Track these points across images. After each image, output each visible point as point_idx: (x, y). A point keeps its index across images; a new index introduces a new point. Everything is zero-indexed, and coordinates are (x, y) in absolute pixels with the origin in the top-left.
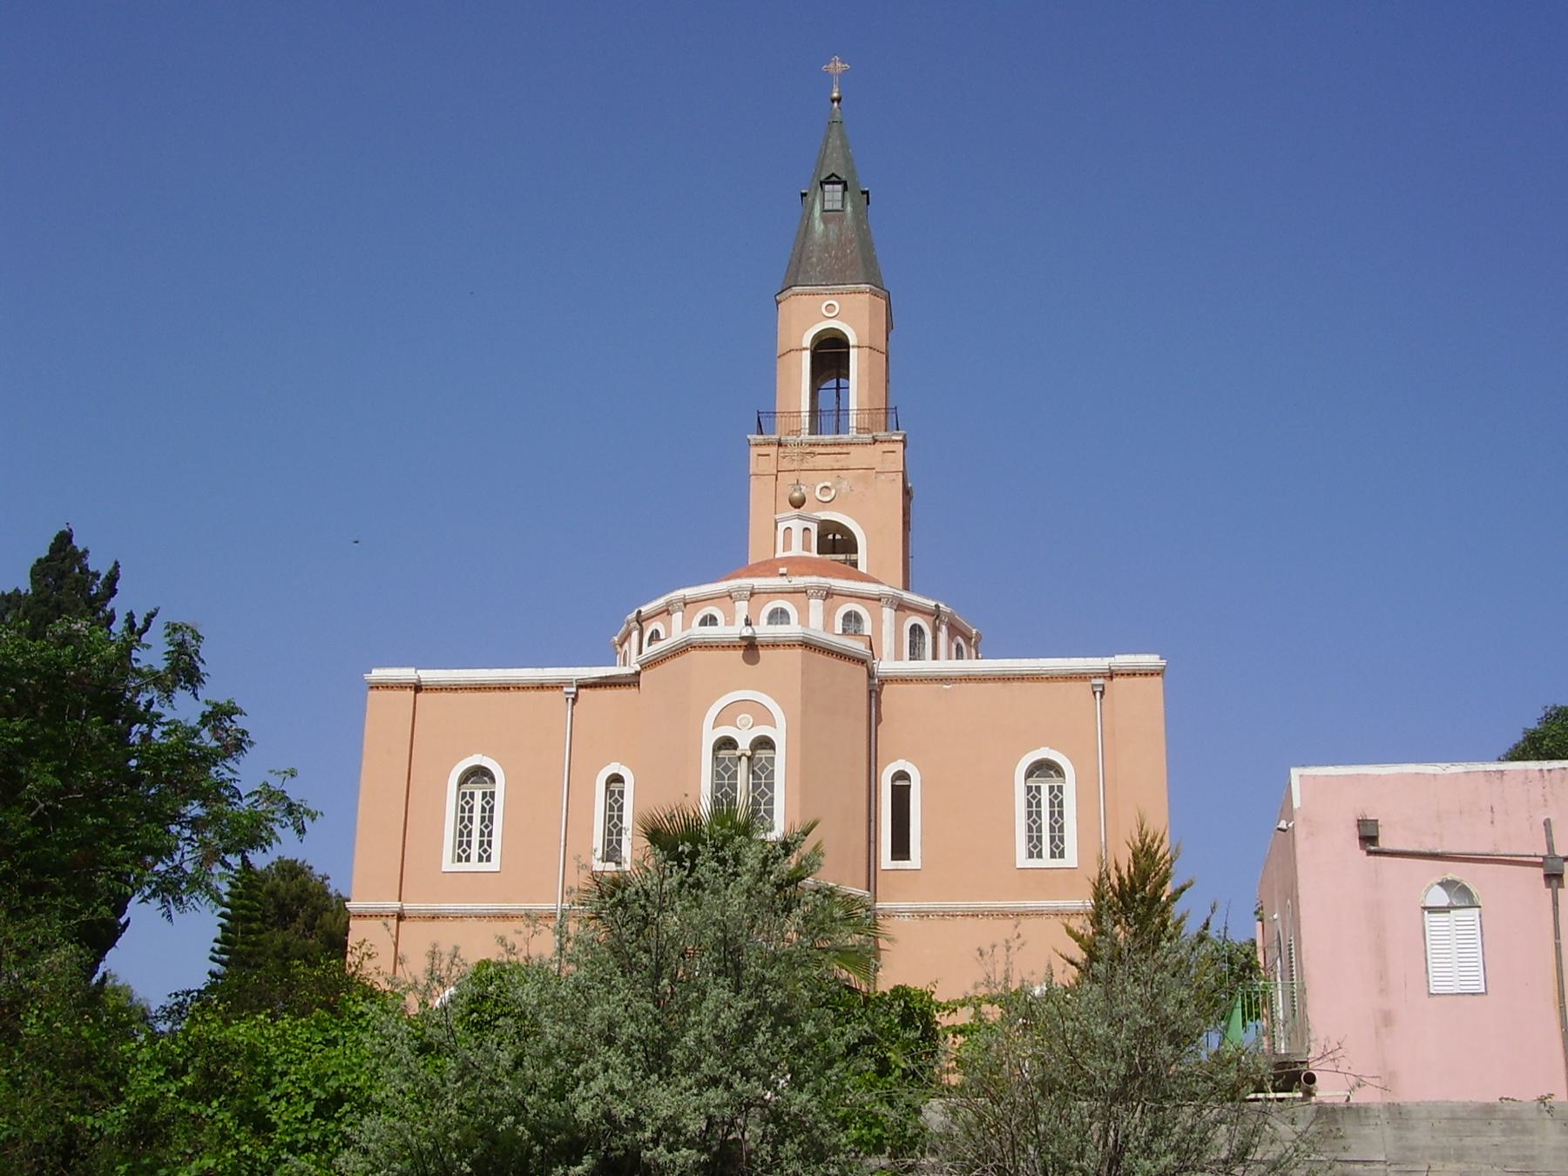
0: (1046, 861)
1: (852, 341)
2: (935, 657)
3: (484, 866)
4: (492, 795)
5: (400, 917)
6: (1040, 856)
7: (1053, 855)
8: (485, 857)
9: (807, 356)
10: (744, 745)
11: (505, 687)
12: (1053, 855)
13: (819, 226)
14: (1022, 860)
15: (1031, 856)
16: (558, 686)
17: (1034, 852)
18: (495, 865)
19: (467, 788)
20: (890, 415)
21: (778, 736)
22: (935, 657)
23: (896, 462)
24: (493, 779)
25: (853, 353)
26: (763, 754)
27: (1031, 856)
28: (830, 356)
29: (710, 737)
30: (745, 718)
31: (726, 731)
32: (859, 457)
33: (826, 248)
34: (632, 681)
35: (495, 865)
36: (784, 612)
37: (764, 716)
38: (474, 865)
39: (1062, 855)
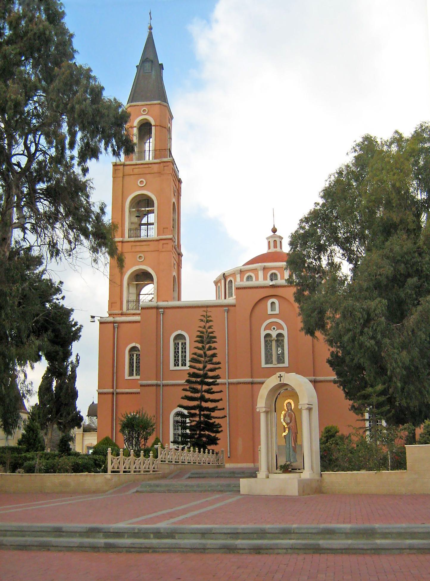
1: (153, 123)
2: (225, 298)
4: (185, 343)
6: (178, 365)
7: (182, 366)
12: (182, 366)
14: (172, 367)
15: (175, 365)
17: (176, 364)
21: (285, 333)
22: (225, 298)
24: (185, 339)
25: (153, 128)
26: (280, 338)
27: (175, 365)
29: (263, 333)
37: (280, 327)
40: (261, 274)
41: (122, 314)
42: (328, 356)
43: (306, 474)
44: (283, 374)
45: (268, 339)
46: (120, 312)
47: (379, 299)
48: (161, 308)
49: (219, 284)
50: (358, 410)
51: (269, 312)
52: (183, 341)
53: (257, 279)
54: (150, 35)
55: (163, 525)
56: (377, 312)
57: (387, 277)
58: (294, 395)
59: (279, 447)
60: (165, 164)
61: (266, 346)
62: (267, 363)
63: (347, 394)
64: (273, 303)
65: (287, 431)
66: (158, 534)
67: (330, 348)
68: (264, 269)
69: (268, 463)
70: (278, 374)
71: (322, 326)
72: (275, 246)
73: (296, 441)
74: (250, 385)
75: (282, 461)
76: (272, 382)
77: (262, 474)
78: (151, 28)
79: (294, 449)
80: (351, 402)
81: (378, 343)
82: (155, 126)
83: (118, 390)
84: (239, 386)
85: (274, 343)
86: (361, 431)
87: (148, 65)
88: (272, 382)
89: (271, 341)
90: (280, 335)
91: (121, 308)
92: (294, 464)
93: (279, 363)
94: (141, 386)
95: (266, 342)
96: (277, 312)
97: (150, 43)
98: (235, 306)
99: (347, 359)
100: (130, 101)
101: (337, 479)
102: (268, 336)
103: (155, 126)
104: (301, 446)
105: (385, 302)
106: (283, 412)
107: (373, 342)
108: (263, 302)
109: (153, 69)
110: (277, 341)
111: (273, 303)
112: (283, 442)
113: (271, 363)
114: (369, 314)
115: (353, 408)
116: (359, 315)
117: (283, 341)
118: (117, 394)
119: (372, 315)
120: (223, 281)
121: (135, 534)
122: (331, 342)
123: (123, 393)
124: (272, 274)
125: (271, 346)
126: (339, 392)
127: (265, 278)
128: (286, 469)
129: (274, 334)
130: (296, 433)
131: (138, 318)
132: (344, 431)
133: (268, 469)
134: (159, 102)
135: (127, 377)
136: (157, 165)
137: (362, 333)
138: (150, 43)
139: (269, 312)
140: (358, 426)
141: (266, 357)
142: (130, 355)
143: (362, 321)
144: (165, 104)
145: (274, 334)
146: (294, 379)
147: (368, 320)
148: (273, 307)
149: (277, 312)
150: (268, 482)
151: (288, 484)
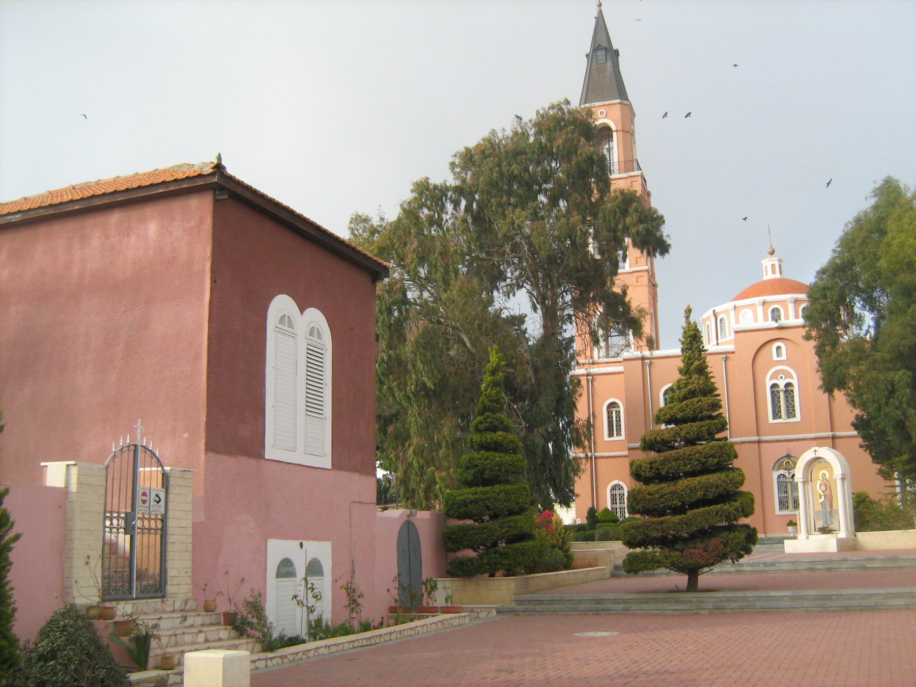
0: (784, 419)
1: (613, 128)
5: (759, 442)
18: (798, 418)
21: (795, 382)
25: (615, 134)
29: (769, 384)
38: (784, 419)
40: (760, 309)
41: (593, 364)
42: (852, 418)
43: (842, 534)
44: (817, 448)
45: (775, 389)
46: (591, 361)
47: (903, 371)
48: (647, 359)
49: (708, 323)
50: (887, 475)
51: (775, 358)
53: (756, 320)
54: (600, 12)
55: (768, 560)
56: (902, 384)
57: (910, 348)
58: (828, 466)
59: (816, 513)
60: (633, 179)
61: (773, 398)
62: (774, 418)
63: (874, 458)
64: (778, 348)
65: (823, 498)
66: (765, 564)
67: (853, 409)
69: (807, 526)
70: (813, 449)
71: (842, 385)
72: (774, 272)
73: (831, 506)
74: (756, 445)
75: (820, 524)
76: (808, 455)
77: (802, 535)
78: (600, 5)
79: (831, 514)
80: (879, 466)
81: (904, 413)
82: (617, 131)
83: (597, 454)
84: (743, 445)
85: (782, 395)
86: (890, 497)
87: (601, 54)
88: (808, 455)
89: (778, 392)
90: (788, 385)
91: (592, 357)
92: (831, 527)
93: (789, 417)
94: (629, 449)
95: (772, 393)
96: (784, 357)
97: (600, 25)
98: (733, 353)
99: (872, 423)
100: (583, 100)
101: (873, 540)
102: (774, 386)
103: (617, 131)
104: (837, 511)
105: (909, 373)
106: (819, 482)
107: (899, 412)
108: (768, 347)
109: (609, 58)
110: (786, 392)
111: (778, 348)
112: (819, 508)
113: (780, 417)
114: (893, 385)
115: (881, 472)
116: (882, 386)
117: (792, 391)
118: (596, 458)
119: (897, 386)
120: (713, 319)
121: (751, 565)
122: (853, 403)
123: (602, 457)
124: (773, 310)
125: (779, 397)
126: (866, 457)
127: (766, 319)
128: (825, 530)
129: (782, 384)
130: (832, 500)
131: (620, 368)
132: (873, 495)
133: (808, 532)
134: (619, 101)
135: (606, 438)
136: (623, 181)
137: (887, 404)
138: (600, 25)
139: (775, 358)
140: (889, 490)
141: (774, 412)
142: (608, 413)
143: (886, 393)
144: (626, 102)
145: (782, 384)
146: (826, 452)
147: (892, 392)
148: (778, 354)
149: (784, 357)
150: (806, 543)
151: (828, 544)
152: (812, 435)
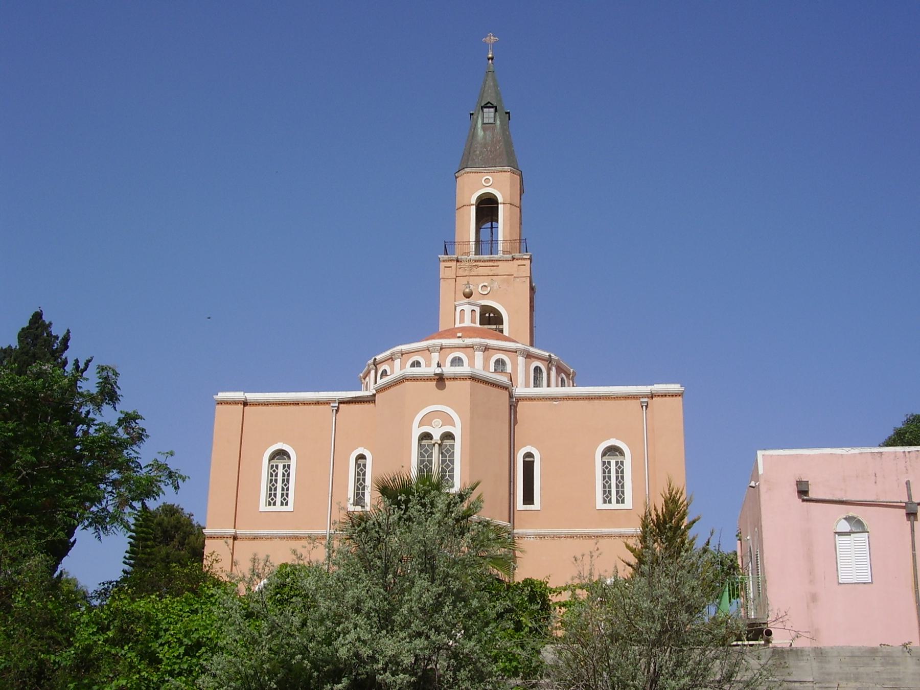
0: (614, 505)
1: (500, 200)
2: (549, 386)
3: (284, 508)
6: (610, 502)
7: (618, 502)
8: (284, 503)
9: (473, 209)
10: (437, 437)
11: (296, 403)
12: (618, 502)
13: (480, 133)
14: (599, 505)
16: (327, 403)
17: (607, 500)
18: (290, 507)
19: (274, 463)
20: (522, 243)
21: (457, 432)
22: (549, 386)
23: (526, 271)
25: (501, 207)
27: (605, 502)
28: (487, 209)
30: (437, 421)
31: (426, 429)
32: (504, 268)
33: (485, 145)
34: (371, 400)
35: (290, 507)
36: (460, 359)
37: (448, 420)
38: (278, 508)
39: (623, 502)
52: (620, 459)
68: (486, 348)
152: (565, 531)
